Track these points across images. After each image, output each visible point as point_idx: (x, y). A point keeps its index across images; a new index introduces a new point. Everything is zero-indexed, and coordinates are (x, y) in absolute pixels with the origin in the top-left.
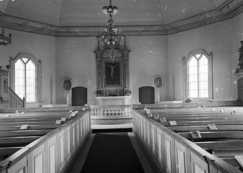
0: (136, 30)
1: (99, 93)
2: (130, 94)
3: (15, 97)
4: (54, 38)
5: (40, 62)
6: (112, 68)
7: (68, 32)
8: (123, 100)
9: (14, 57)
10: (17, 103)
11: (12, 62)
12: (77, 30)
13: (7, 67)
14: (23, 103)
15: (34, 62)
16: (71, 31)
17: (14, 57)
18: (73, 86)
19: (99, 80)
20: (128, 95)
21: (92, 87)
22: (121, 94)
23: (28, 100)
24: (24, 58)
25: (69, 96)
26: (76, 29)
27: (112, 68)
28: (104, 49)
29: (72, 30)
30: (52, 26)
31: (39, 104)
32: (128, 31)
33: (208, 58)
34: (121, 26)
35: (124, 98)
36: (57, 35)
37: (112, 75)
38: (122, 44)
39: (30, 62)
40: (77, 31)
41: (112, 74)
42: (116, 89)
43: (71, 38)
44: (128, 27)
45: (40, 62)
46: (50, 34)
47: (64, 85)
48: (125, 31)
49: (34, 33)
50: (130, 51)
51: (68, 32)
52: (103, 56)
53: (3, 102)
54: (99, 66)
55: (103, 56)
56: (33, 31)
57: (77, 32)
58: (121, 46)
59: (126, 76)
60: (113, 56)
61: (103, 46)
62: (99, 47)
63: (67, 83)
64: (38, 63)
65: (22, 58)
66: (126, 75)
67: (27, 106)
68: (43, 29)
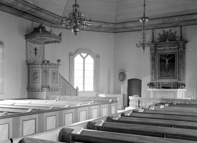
0: (194, 18)
1: (151, 85)
2: (185, 87)
3: (69, 86)
4: (114, 34)
5: (98, 56)
6: (167, 60)
7: (124, 28)
8: (175, 93)
9: (73, 53)
10: (71, 91)
11: (71, 57)
12: (131, 25)
13: (57, 61)
14: (77, 92)
15: (92, 56)
16: (126, 26)
17: (73, 53)
18: (129, 76)
19: (153, 72)
20: (182, 88)
21: (146, 80)
22: (175, 86)
23: (79, 90)
24: (83, 53)
25: (124, 87)
26: (130, 24)
27: (167, 60)
28: (159, 42)
29: (127, 25)
30: (107, 23)
31: (96, 93)
32: (185, 21)
33: (94, 59)
34: (175, 16)
35: (177, 91)
36: (116, 31)
37: (167, 67)
38: (178, 34)
39: (89, 56)
40: (132, 25)
41: (166, 66)
42: (171, 81)
43: (129, 32)
44: (184, 16)
45: (98, 56)
46: (108, 31)
47: (119, 77)
48: (181, 21)
49: (92, 31)
50: (186, 42)
51: (124, 28)
52: (158, 48)
53: (51, 90)
54: (153, 59)
55: (158, 48)
56: (92, 29)
57: (132, 27)
58: (178, 37)
59: (181, 68)
60: (167, 49)
61: (157, 39)
62: (153, 40)
63: (122, 75)
64: (96, 58)
65: (82, 54)
66: (181, 67)
67: (80, 95)
68: (100, 27)
